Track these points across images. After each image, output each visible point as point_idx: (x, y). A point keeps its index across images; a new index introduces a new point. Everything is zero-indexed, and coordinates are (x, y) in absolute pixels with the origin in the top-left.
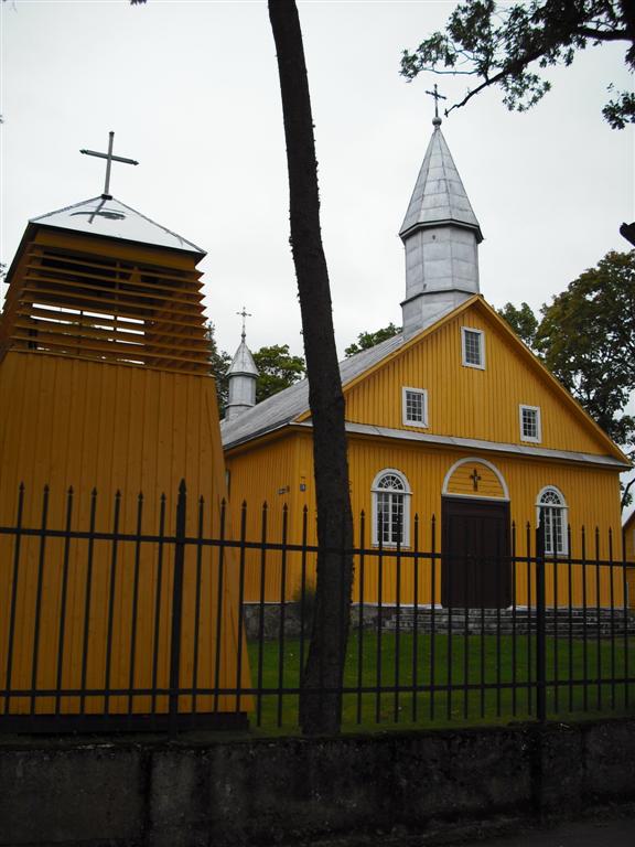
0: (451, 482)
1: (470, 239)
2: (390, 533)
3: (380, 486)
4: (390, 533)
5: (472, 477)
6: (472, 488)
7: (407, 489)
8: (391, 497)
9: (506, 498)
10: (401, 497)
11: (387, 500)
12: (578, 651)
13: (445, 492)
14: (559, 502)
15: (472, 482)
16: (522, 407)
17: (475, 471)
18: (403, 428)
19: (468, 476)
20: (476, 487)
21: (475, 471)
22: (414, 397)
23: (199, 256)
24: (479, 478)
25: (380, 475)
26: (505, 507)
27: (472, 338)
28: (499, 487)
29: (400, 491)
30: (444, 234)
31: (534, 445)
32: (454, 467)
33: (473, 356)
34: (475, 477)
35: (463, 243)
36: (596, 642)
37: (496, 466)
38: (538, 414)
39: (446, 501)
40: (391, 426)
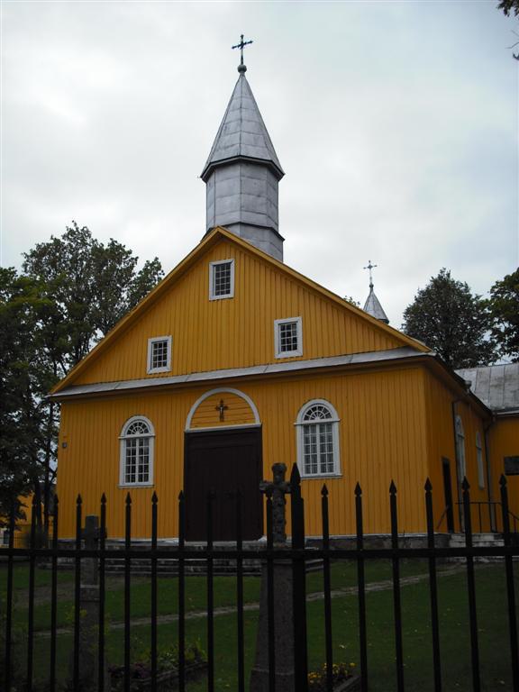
0: (195, 418)
1: (265, 174)
2: (319, 464)
3: (306, 418)
4: (319, 464)
5: (218, 409)
6: (218, 419)
7: (335, 417)
8: (318, 429)
9: (257, 423)
10: (330, 424)
11: (134, 445)
12: (43, 599)
13: (188, 428)
14: (329, 416)
15: (218, 413)
16: (169, 339)
17: (222, 402)
18: (279, 361)
19: (213, 408)
20: (222, 417)
21: (222, 402)
22: (160, 346)
23: (157, 259)
24: (226, 408)
25: (304, 409)
26: (256, 433)
27: (223, 272)
28: (250, 412)
29: (328, 420)
30: (235, 172)
31: (297, 359)
32: (198, 403)
33: (223, 286)
34: (222, 408)
35: (228, 179)
36: (233, 579)
37: (248, 394)
38: (299, 325)
39: (190, 437)
40: (143, 376)
